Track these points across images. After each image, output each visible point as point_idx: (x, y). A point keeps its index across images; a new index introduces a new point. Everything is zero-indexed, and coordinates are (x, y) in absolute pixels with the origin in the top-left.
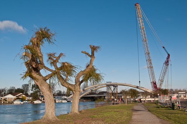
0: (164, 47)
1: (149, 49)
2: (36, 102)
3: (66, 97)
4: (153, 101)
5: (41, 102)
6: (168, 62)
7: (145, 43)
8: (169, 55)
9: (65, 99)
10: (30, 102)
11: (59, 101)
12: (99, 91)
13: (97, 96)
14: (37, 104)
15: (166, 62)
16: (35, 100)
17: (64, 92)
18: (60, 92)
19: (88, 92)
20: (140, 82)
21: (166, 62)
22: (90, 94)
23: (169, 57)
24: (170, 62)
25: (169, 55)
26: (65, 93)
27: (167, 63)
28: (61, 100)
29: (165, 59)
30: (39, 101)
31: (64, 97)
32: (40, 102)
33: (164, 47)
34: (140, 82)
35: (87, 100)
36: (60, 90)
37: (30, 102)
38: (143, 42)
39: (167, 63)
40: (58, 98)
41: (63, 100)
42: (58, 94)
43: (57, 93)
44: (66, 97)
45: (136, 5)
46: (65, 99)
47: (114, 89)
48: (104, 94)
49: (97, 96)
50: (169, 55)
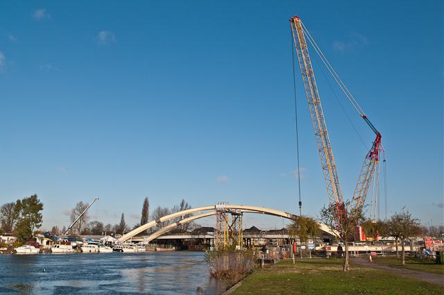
0: (364, 117)
1: (328, 136)
2: (21, 250)
3: (110, 239)
4: (375, 254)
5: (38, 250)
6: (376, 153)
7: (315, 107)
8: (379, 136)
9: (109, 244)
10: (6, 249)
11: (89, 249)
12: (195, 225)
13: (190, 237)
14: (26, 257)
15: (371, 153)
16: (21, 246)
17: (109, 226)
18: (100, 226)
19: (169, 227)
20: (300, 203)
21: (371, 153)
22: (173, 232)
23: (380, 139)
24: (381, 154)
25: (380, 137)
26: (111, 230)
27: (374, 154)
28: (96, 246)
29: (370, 146)
30: (33, 247)
31: (106, 237)
32: (35, 251)
33: (364, 117)
34: (300, 203)
35: (165, 247)
36: (100, 221)
37: (6, 249)
38: (321, 154)
39: (374, 154)
40: (90, 240)
41: (102, 245)
42: (93, 230)
43: (91, 227)
44: (110, 239)
45: (293, 21)
46: (109, 244)
47: (234, 222)
48: (209, 233)
49: (190, 237)
50: (379, 136)
